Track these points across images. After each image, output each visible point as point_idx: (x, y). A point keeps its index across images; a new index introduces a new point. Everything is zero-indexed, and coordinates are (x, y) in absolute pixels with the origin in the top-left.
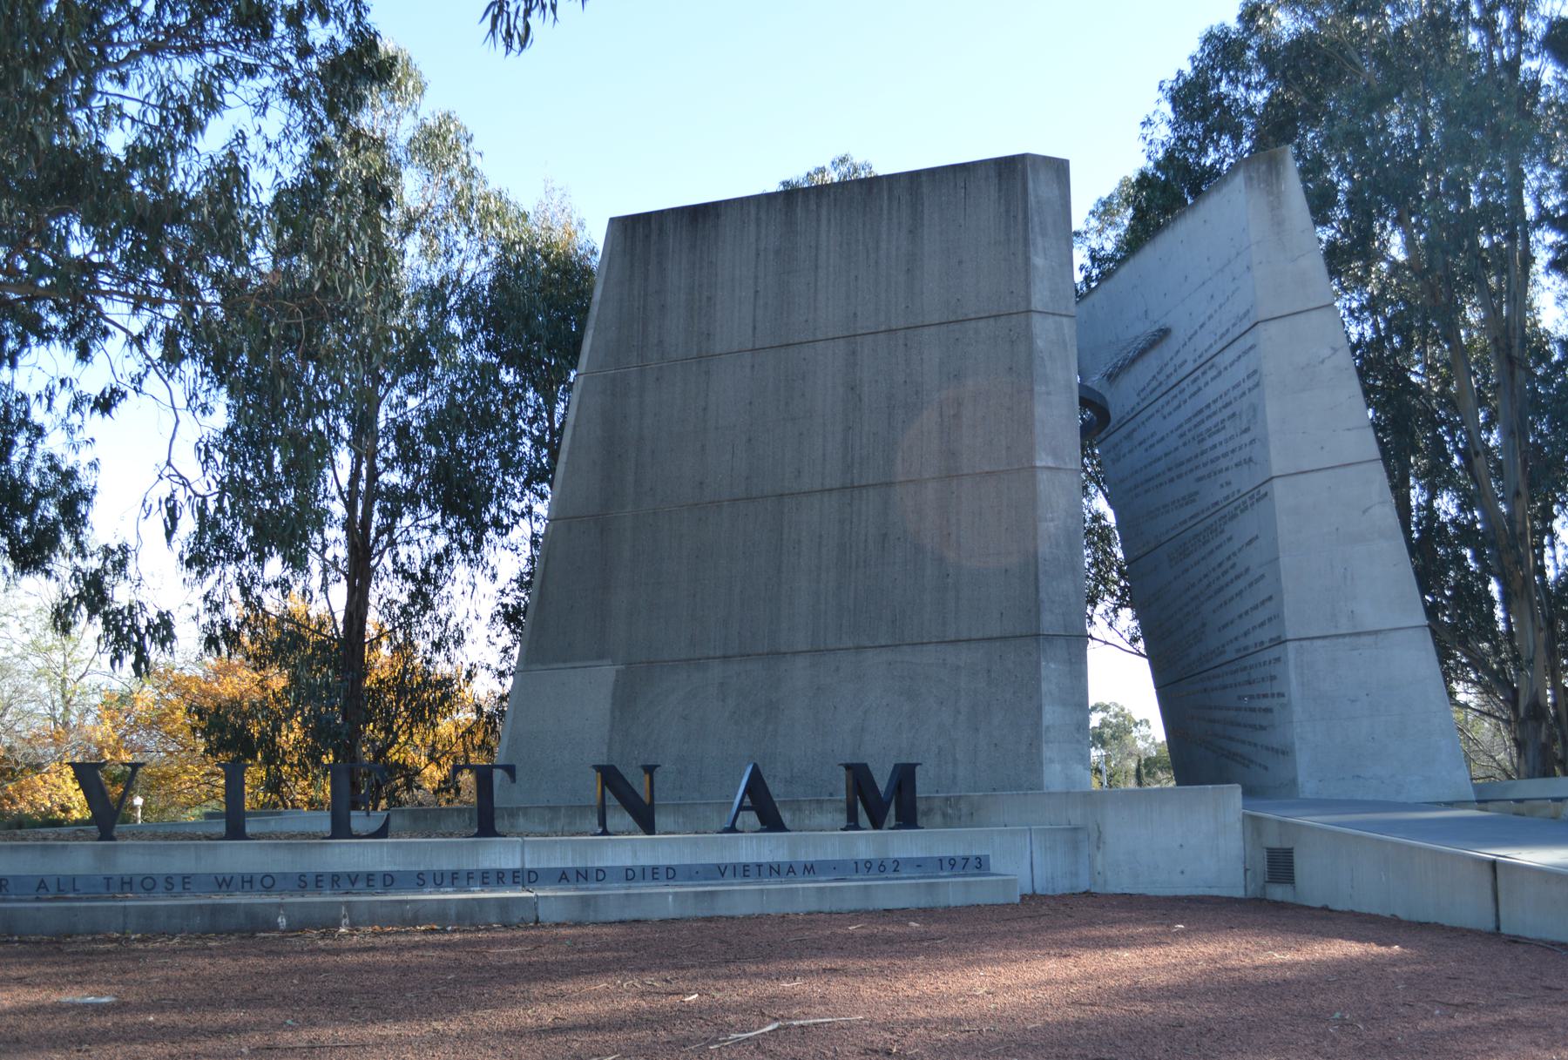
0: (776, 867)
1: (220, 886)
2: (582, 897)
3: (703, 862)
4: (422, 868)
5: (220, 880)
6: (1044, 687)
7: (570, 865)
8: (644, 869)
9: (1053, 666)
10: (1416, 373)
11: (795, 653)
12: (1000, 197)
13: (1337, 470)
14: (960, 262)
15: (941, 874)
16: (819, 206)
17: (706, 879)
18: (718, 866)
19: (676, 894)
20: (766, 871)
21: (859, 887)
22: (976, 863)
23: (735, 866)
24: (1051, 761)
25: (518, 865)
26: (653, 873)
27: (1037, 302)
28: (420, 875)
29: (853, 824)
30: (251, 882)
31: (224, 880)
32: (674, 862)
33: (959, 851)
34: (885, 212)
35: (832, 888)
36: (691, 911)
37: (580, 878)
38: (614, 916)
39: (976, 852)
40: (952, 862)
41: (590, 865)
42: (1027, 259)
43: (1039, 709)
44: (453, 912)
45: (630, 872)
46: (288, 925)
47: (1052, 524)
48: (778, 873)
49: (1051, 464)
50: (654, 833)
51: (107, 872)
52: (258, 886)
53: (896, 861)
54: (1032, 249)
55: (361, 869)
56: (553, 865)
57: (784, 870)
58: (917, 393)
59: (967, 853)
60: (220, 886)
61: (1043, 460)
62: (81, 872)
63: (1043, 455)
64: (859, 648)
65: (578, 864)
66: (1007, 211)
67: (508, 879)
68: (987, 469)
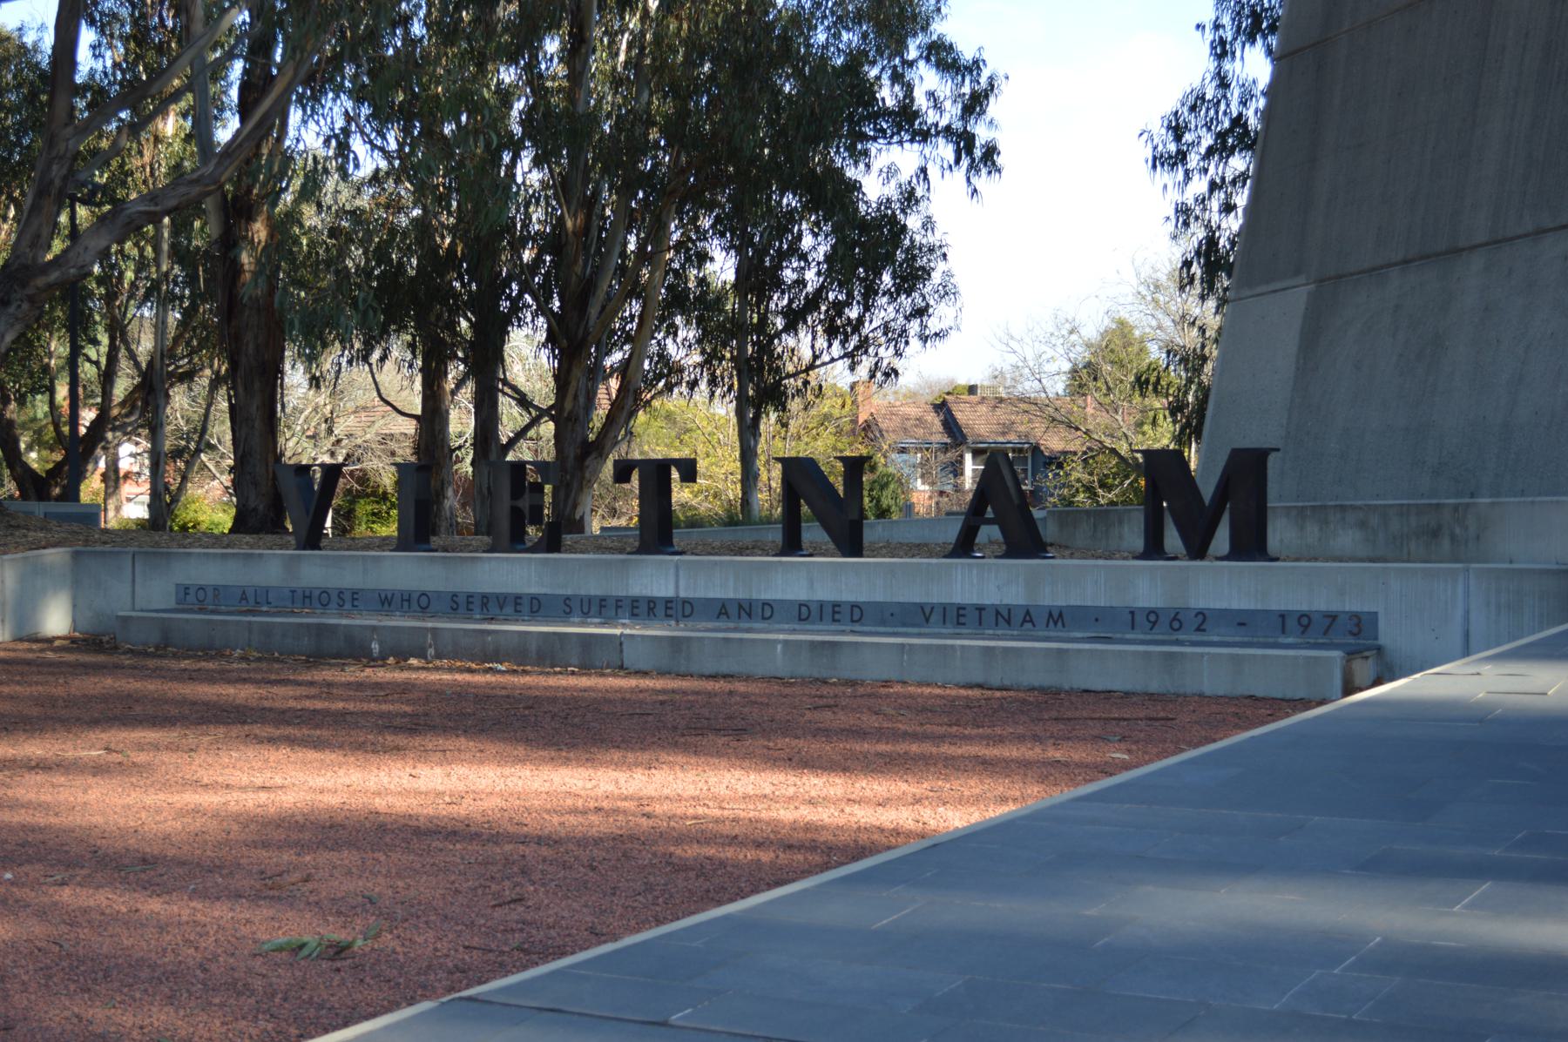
0: (746, 607)
1: (383, 604)
2: (673, 638)
3: (901, 599)
4: (569, 592)
5: (383, 596)
7: (731, 596)
8: (822, 604)
10: (73, 217)
15: (1282, 640)
17: (904, 625)
18: (922, 607)
19: (786, 642)
20: (989, 617)
21: (1135, 653)
23: (945, 608)
25: (670, 593)
26: (856, 614)
28: (567, 600)
29: (1154, 548)
30: (409, 600)
31: (1056, 623)
32: (862, 598)
33: (1321, 602)
35: (1006, 649)
36: (806, 668)
37: (743, 614)
38: (709, 668)
39: (1352, 605)
40: (1305, 621)
41: (755, 596)
44: (533, 647)
45: (804, 609)
46: (380, 652)
48: (1008, 622)
50: (860, 555)
51: (294, 585)
52: (415, 606)
53: (1201, 614)
55: (510, 591)
56: (711, 595)
57: (1018, 617)
59: (1335, 607)
60: (383, 604)
62: (274, 583)
64: (1540, 232)
65: (741, 596)
67: (660, 610)
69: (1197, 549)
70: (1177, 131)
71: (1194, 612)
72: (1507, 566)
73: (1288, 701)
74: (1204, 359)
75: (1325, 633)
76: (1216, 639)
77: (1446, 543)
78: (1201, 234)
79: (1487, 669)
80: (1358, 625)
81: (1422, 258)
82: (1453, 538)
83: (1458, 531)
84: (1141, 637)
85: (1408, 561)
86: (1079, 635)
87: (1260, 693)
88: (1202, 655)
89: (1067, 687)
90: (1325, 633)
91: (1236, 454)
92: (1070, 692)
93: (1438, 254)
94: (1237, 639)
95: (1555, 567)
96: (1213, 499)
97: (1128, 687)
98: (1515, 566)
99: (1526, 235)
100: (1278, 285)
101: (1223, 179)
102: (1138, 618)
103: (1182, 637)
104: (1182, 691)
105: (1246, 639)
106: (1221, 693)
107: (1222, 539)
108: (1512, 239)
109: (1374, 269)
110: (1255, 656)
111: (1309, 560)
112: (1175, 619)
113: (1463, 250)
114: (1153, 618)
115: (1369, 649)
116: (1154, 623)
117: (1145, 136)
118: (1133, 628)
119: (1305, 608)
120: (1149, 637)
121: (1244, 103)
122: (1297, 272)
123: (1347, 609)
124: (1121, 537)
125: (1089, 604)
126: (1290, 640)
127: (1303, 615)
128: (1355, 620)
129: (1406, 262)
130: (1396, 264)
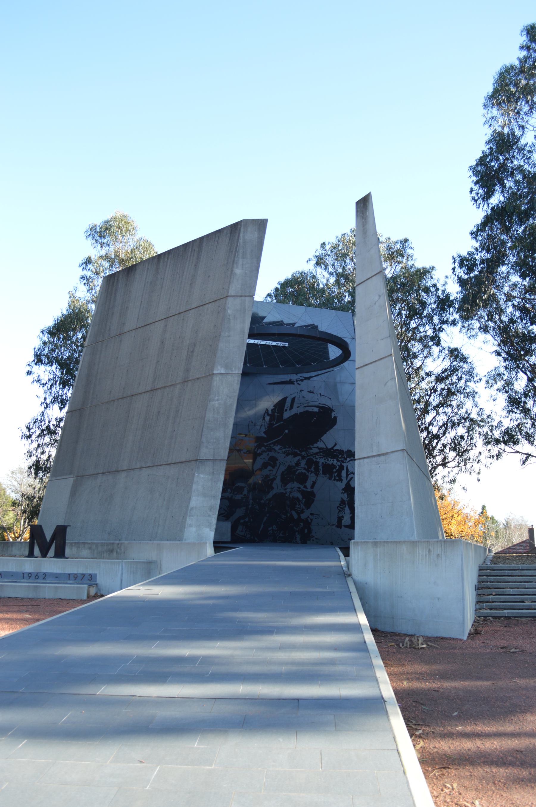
6: (194, 487)
9: (202, 476)
11: (123, 471)
12: (229, 243)
13: (377, 363)
14: (209, 277)
15: (69, 582)
16: (168, 259)
22: (89, 577)
24: (191, 526)
27: (232, 292)
29: (31, 554)
33: (81, 570)
34: (189, 258)
42: (232, 270)
43: (190, 499)
47: (217, 402)
49: (223, 372)
53: (45, 574)
54: (235, 266)
58: (182, 342)
61: (219, 370)
63: (219, 367)
64: (142, 468)
66: (230, 249)
68: (197, 376)
69: (44, 554)
70: (29, 428)
71: (42, 574)
72: (133, 561)
73: (71, 600)
74: (34, 497)
75: (82, 580)
76: (49, 581)
77: (115, 554)
78: (443, 457)
79: (141, 588)
80: (91, 577)
81: (108, 472)
82: (117, 552)
83: (118, 551)
84: (26, 581)
85: (103, 559)
86: (6, 580)
87: (63, 598)
88: (46, 586)
89: (3, 596)
90: (82, 580)
91: (58, 527)
92: (4, 598)
93: (113, 472)
94: (55, 582)
95: (146, 561)
96: (50, 540)
97: (22, 596)
98: (134, 561)
99: (138, 468)
100: (65, 477)
101: (43, 443)
102: (25, 575)
103: (39, 581)
104: (39, 597)
105: (58, 582)
106: (51, 598)
107: (52, 552)
108: (134, 469)
109: (94, 475)
110: (62, 586)
111: (76, 558)
112: (37, 575)
113: (120, 471)
114: (30, 575)
115: (94, 584)
116: (30, 577)
117: (20, 429)
118: (23, 578)
119: (76, 572)
120: (28, 581)
121: (49, 422)
122: (70, 474)
123: (88, 573)
124: (12, 551)
125: (10, 571)
126: (71, 582)
127: (75, 574)
128: (90, 576)
129: (103, 473)
130: (100, 474)
